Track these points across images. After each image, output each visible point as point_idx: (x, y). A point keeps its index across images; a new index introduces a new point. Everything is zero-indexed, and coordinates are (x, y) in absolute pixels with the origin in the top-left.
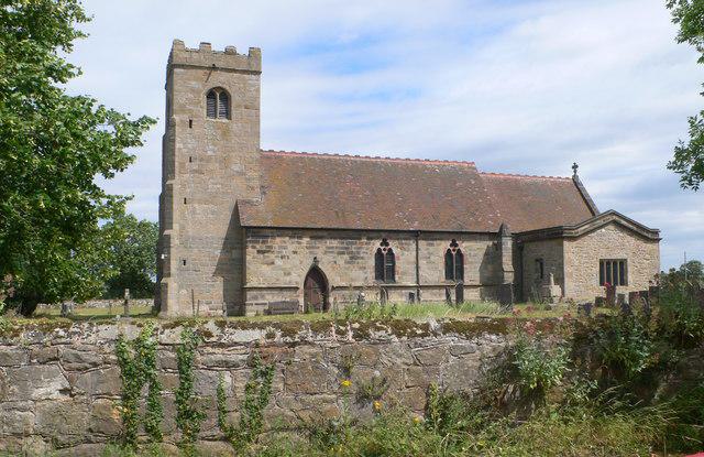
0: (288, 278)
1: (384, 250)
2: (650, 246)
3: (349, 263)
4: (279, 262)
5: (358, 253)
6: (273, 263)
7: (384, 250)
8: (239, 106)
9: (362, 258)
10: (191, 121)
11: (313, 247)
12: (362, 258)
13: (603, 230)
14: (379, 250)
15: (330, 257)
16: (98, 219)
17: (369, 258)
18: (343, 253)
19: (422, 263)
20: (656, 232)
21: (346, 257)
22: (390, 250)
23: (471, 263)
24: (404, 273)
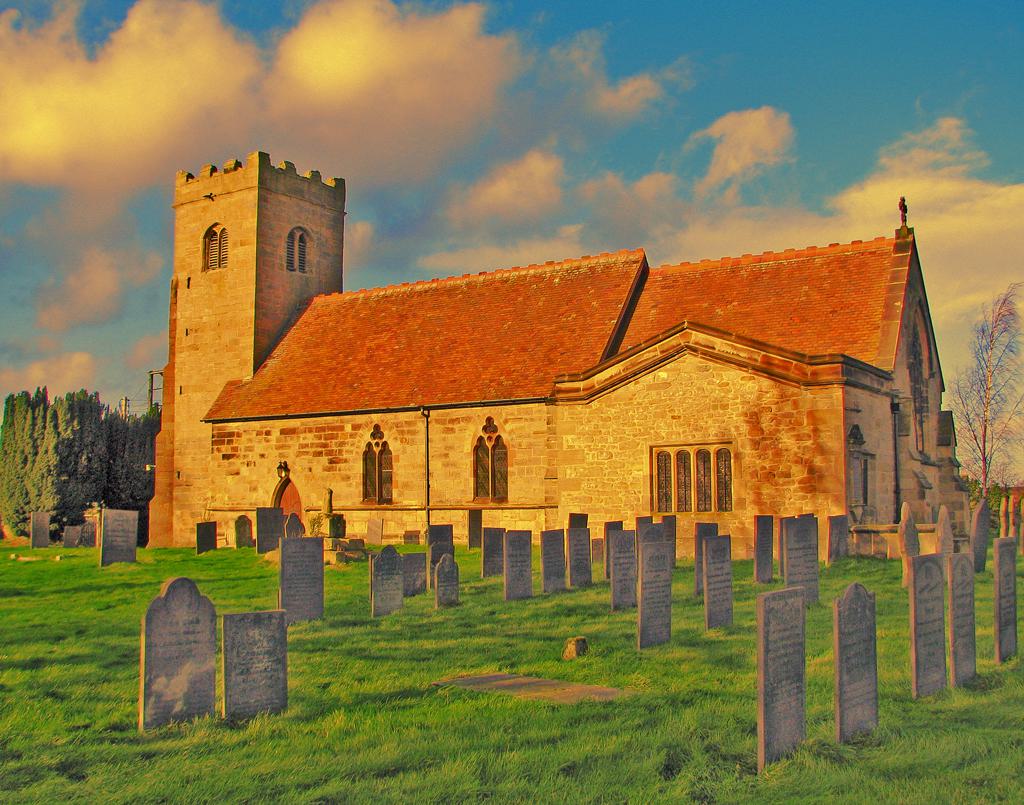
0: (255, 495)
1: (377, 444)
2: (180, 284)
3: (329, 470)
4: (244, 471)
5: (340, 452)
6: (238, 473)
7: (377, 444)
8: (235, 245)
9: (346, 461)
10: (189, 279)
11: (282, 447)
12: (346, 461)
13: (662, 374)
14: (369, 445)
15: (304, 461)
16: (977, 585)
17: (355, 460)
18: (320, 454)
19: (436, 465)
20: (222, 261)
21: (324, 460)
22: (385, 444)
23: (522, 463)
24: (406, 485)
